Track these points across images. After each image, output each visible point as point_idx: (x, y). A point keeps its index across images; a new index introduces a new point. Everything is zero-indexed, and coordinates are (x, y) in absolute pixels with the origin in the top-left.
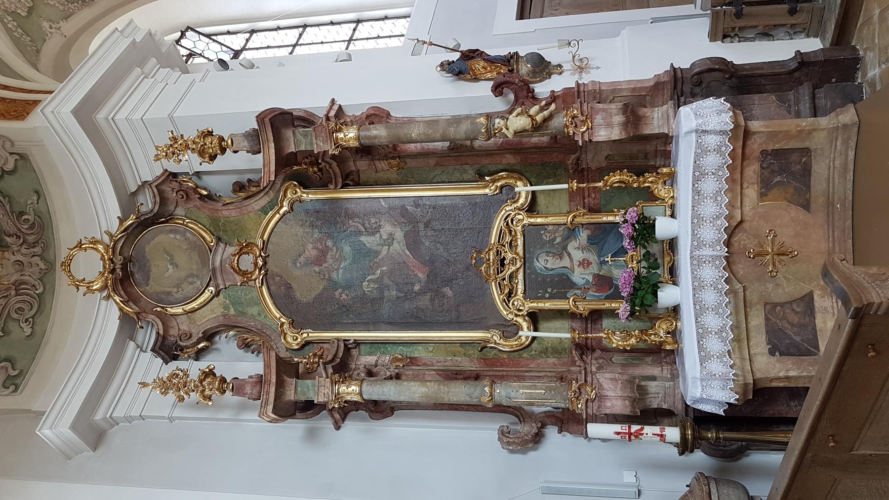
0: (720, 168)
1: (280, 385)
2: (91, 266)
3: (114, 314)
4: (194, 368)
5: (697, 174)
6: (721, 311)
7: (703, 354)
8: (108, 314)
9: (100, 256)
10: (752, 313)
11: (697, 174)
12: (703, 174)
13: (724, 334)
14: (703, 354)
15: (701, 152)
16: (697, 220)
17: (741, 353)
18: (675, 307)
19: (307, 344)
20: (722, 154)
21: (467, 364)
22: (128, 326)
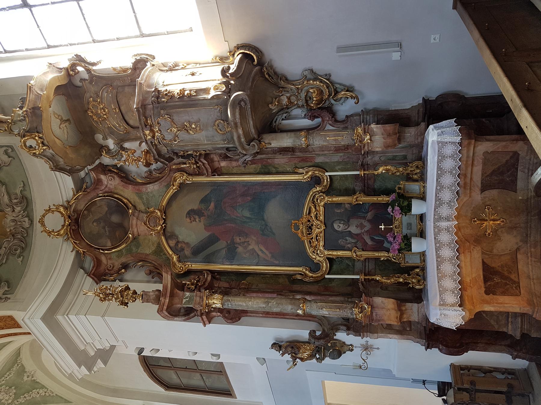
0: (454, 168)
1: (172, 295)
2: (56, 221)
3: (71, 257)
4: (119, 285)
5: (438, 203)
6: (453, 245)
7: (439, 172)
8: (65, 254)
9: (63, 224)
10: (475, 169)
11: (438, 245)
12: (442, 187)
13: (453, 204)
14: (439, 260)
15: (441, 158)
16: (439, 202)
17: (468, 151)
18: (422, 214)
19: (189, 273)
20: (454, 175)
22: (79, 263)
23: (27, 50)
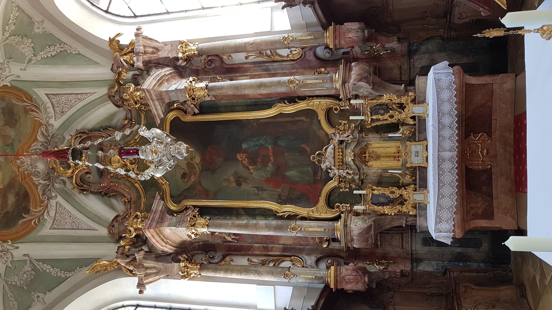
21: (382, 200)
23: (168, 13)
